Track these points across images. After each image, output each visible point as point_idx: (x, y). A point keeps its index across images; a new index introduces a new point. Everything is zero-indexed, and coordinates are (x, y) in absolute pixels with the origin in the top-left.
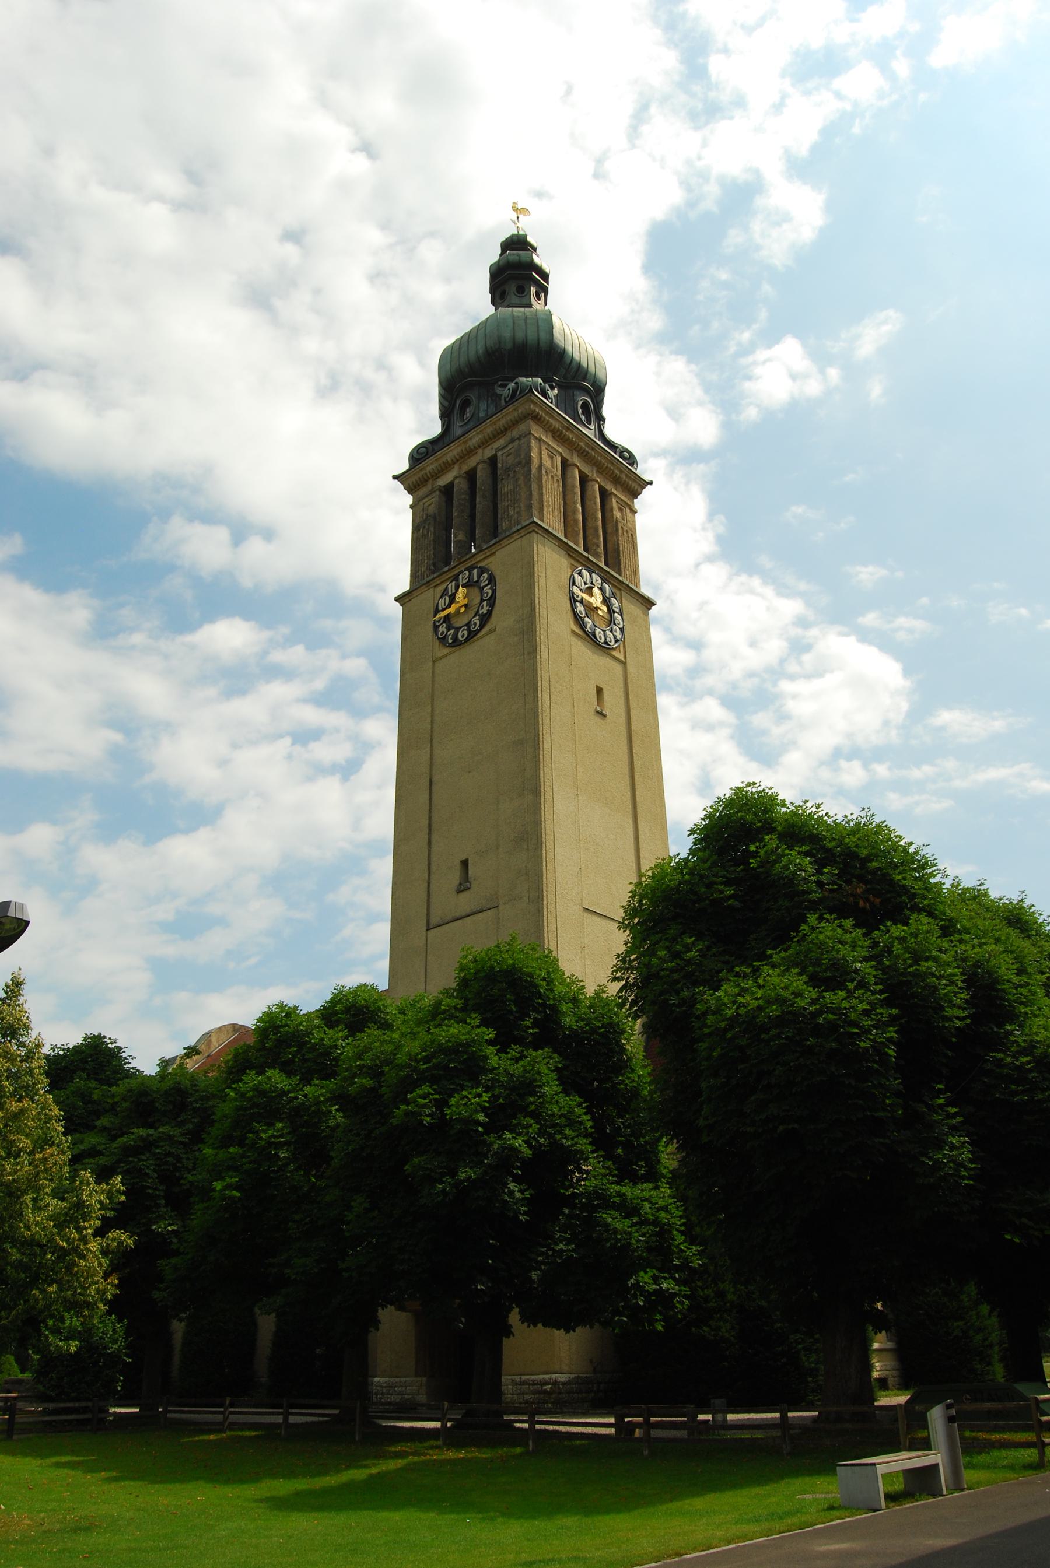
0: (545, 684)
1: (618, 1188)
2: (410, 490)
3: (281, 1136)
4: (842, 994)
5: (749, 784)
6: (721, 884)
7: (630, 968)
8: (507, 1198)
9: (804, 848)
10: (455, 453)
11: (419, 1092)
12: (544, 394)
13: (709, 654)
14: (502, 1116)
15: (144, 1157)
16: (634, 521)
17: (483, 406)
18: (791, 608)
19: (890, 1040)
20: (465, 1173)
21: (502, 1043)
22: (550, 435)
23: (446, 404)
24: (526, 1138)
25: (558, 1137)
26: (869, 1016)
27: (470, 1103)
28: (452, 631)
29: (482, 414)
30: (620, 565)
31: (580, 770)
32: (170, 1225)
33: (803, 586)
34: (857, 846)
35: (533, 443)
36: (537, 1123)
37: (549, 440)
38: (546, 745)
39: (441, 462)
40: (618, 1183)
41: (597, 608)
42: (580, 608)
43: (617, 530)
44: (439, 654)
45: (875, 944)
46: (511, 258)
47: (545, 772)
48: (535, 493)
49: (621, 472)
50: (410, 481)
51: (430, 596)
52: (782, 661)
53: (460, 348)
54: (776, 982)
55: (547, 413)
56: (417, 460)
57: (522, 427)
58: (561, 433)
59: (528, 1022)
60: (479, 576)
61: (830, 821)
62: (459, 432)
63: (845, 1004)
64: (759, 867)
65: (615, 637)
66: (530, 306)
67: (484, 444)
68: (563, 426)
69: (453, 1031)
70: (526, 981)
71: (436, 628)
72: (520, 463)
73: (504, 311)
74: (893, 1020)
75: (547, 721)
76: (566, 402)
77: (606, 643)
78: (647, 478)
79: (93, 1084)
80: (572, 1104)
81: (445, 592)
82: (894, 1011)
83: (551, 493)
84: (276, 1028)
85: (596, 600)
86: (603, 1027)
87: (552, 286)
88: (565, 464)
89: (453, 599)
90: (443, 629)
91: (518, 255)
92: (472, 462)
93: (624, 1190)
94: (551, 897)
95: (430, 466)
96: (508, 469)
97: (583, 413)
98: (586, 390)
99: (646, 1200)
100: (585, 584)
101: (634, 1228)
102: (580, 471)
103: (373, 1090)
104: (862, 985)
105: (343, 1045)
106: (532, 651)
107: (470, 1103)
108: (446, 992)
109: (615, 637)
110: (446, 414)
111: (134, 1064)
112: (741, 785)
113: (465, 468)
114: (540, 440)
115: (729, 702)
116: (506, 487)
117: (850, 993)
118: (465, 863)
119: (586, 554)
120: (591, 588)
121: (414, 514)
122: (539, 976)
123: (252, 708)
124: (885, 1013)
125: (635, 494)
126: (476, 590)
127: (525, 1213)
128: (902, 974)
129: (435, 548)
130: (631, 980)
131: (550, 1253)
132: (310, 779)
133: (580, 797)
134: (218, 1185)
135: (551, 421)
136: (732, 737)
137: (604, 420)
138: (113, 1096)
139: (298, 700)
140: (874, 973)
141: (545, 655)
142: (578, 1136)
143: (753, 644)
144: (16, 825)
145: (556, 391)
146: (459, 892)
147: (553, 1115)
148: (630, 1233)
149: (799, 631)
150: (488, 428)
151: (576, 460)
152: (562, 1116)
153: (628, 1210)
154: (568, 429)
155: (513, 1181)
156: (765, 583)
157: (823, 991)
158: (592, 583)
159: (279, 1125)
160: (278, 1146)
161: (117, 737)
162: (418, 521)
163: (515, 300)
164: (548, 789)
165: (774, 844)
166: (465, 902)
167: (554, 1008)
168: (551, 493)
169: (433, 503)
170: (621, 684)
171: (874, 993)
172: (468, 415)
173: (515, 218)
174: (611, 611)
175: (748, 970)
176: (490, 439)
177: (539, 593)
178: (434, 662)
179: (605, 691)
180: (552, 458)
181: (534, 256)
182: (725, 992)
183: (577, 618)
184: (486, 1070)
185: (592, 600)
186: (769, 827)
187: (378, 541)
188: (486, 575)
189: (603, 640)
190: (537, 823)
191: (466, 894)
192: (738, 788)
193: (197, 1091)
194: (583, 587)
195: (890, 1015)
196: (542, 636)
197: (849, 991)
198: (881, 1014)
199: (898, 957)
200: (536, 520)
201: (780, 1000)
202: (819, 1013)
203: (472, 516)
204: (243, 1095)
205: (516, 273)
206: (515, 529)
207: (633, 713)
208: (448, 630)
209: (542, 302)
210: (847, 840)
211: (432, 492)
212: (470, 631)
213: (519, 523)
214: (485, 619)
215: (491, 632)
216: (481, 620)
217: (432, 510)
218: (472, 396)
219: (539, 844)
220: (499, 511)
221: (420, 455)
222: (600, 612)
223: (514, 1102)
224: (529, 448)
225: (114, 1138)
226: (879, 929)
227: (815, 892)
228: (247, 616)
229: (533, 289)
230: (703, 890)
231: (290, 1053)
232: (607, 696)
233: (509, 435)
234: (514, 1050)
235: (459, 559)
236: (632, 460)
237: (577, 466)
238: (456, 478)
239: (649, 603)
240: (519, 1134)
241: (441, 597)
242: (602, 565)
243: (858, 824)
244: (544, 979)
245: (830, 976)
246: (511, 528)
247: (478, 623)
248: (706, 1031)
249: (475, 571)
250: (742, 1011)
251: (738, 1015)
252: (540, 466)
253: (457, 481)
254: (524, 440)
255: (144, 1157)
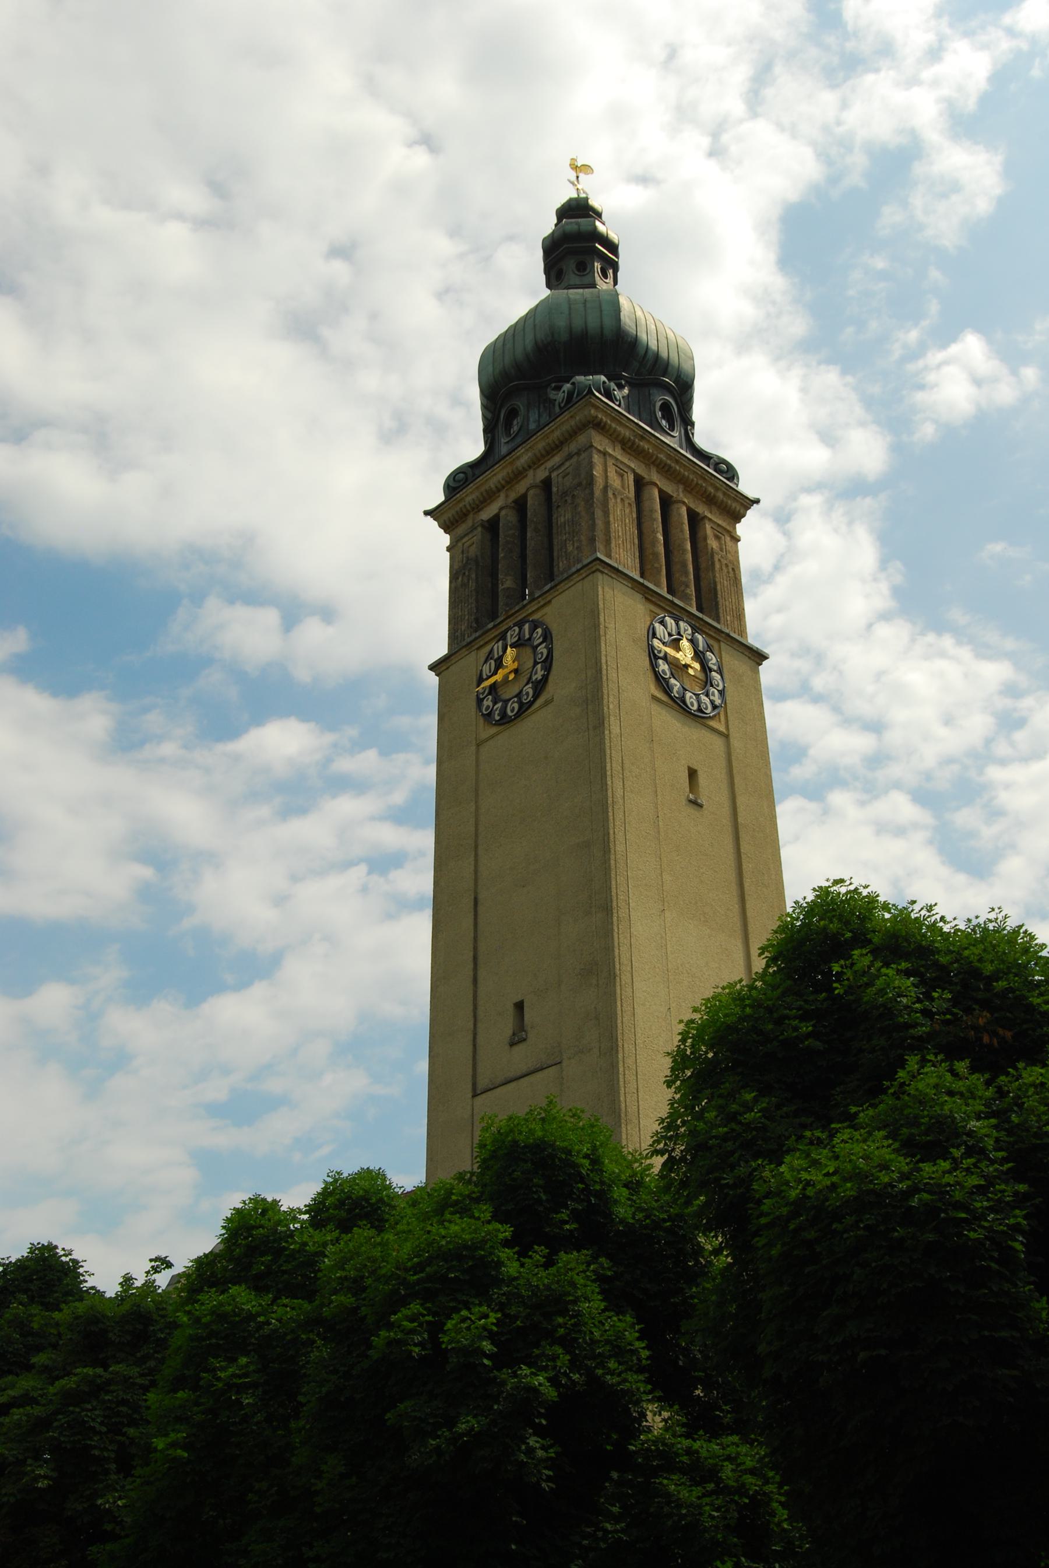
0: (617, 767)
1: (686, 1443)
2: (447, 527)
3: (246, 1375)
4: (945, 1165)
5: (837, 882)
6: (795, 1018)
7: (675, 1138)
8: (523, 1457)
9: (904, 965)
10: (500, 477)
11: (405, 1312)
12: (609, 395)
13: (894, 738)
14: (516, 1344)
15: (89, 1406)
16: (737, 552)
17: (533, 416)
18: (995, 672)
19: (1016, 1228)
20: (467, 1423)
21: (521, 1244)
22: (618, 447)
23: (489, 416)
24: (551, 1374)
25: (599, 1372)
26: (984, 1194)
27: (473, 1325)
28: (499, 705)
29: (532, 426)
30: (717, 609)
31: (666, 877)
32: (120, 1498)
33: (1010, 644)
34: (981, 960)
35: (596, 458)
36: (567, 1352)
37: (618, 453)
38: (619, 848)
39: (483, 489)
40: (687, 1436)
41: (687, 666)
42: (663, 666)
43: (713, 564)
44: (484, 735)
45: (1001, 1093)
46: (568, 228)
47: (618, 883)
48: (600, 523)
49: (717, 489)
50: (445, 517)
51: (472, 662)
52: (988, 742)
53: (504, 345)
54: (858, 1151)
55: (613, 419)
56: (454, 489)
57: (582, 439)
58: (634, 443)
59: (564, 1215)
60: (532, 631)
61: (946, 928)
62: (504, 450)
63: (948, 1179)
64: (846, 992)
65: (712, 702)
66: (593, 285)
67: (536, 463)
68: (636, 435)
69: (454, 1228)
70: (560, 1159)
71: (480, 701)
72: (580, 484)
73: (562, 293)
74: (1020, 1200)
75: (619, 816)
76: (640, 404)
77: (700, 710)
78: (751, 494)
79: (35, 1309)
80: (625, 1327)
81: (489, 657)
82: (1022, 1188)
83: (621, 520)
84: (250, 1228)
85: (685, 655)
86: (670, 1219)
87: (625, 259)
88: (640, 484)
89: (499, 664)
90: (488, 702)
91: (578, 224)
92: (521, 488)
93: (696, 1445)
94: (628, 1047)
95: (470, 495)
96: (565, 493)
97: (663, 417)
98: (667, 388)
99: (729, 1458)
100: (670, 635)
101: (707, 1500)
102: (661, 491)
103: (355, 1310)
104: (976, 1150)
105: (332, 1250)
106: (599, 724)
107: (473, 1325)
108: (460, 1177)
109: (712, 702)
110: (490, 431)
111: (90, 1282)
112: (827, 884)
113: (513, 496)
114: (605, 454)
115: (922, 797)
116: (563, 516)
117: (956, 1164)
118: (519, 1006)
119: (670, 597)
120: (679, 640)
121: (452, 558)
122: (579, 1152)
123: (314, 830)
124: (1008, 1190)
125: (738, 517)
126: (528, 651)
127: (549, 1479)
128: (1036, 1135)
129: (477, 601)
130: (677, 1154)
131: (600, 1534)
132: (390, 916)
133: (667, 914)
134: (160, 1443)
135: (619, 428)
136: (930, 842)
137: (692, 424)
138: (57, 1324)
139: (373, 818)
140: (995, 1133)
141: (615, 730)
142: (626, 1371)
143: (948, 721)
144: (22, 985)
145: (626, 391)
146: (512, 1044)
147: (593, 1342)
148: (700, 1506)
149: (1008, 702)
150: (539, 444)
151: (655, 477)
152: (608, 1342)
153: (700, 1472)
154: (642, 438)
155: (535, 1434)
156: (959, 643)
157: (918, 1162)
158: (679, 634)
159: (243, 1360)
160: (240, 1389)
161: (146, 873)
162: (456, 567)
163: (575, 280)
164: (622, 904)
165: (866, 961)
166: (520, 1058)
167: (601, 1195)
168: (621, 520)
169: (475, 540)
170: (723, 763)
171: (992, 1162)
172: (515, 428)
173: (574, 179)
174: (705, 668)
175: (824, 1136)
176: (543, 456)
177: (607, 649)
178: (478, 745)
179: (700, 773)
180: (622, 476)
181: (598, 223)
182: (792, 1166)
183: (661, 681)
184: (498, 1282)
185: (679, 655)
186: (861, 939)
187: (407, 596)
188: (539, 630)
189: (695, 707)
190: (608, 950)
191: (521, 1047)
192: (821, 888)
193: (163, 1316)
194: (667, 639)
195: (1016, 1194)
196: (610, 705)
197: (954, 1159)
198: (1002, 1191)
199: (1032, 1111)
200: (599, 555)
201: (858, 1176)
202: (914, 1190)
203: (523, 557)
204: (198, 1320)
205: (578, 246)
206: (574, 569)
207: (741, 800)
208: (495, 703)
209: (610, 280)
210: (966, 953)
211: (473, 528)
212: (521, 704)
213: (579, 561)
214: (540, 687)
215: (547, 703)
216: (535, 689)
217: (473, 551)
218: (520, 403)
219: (612, 977)
220: (556, 548)
221: (459, 482)
222: (691, 672)
223: (534, 1325)
224: (591, 465)
225: (53, 1380)
226: (1008, 1074)
227: (922, 1025)
228: (304, 716)
229: (597, 265)
230: (770, 1027)
231: (262, 1263)
232: (702, 780)
233: (566, 450)
234: (539, 1253)
235: (507, 611)
236: (731, 473)
237: (656, 485)
238: (501, 509)
239: (759, 657)
240: (545, 1369)
241: (485, 662)
242: (693, 610)
243: (985, 930)
244: (587, 1156)
245: (931, 1140)
246: (570, 568)
247: (531, 692)
248: (763, 1221)
249: (527, 627)
250: (810, 1192)
251: (806, 1197)
252: (606, 487)
253: (503, 513)
254: (583, 455)
255: (89, 1406)
